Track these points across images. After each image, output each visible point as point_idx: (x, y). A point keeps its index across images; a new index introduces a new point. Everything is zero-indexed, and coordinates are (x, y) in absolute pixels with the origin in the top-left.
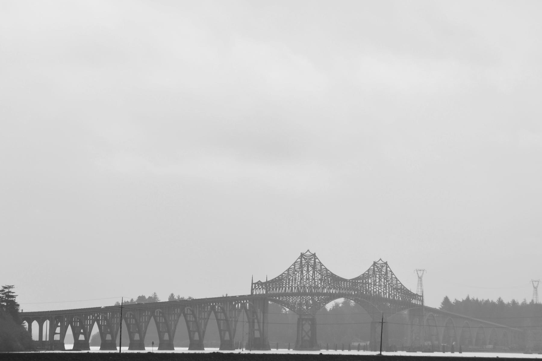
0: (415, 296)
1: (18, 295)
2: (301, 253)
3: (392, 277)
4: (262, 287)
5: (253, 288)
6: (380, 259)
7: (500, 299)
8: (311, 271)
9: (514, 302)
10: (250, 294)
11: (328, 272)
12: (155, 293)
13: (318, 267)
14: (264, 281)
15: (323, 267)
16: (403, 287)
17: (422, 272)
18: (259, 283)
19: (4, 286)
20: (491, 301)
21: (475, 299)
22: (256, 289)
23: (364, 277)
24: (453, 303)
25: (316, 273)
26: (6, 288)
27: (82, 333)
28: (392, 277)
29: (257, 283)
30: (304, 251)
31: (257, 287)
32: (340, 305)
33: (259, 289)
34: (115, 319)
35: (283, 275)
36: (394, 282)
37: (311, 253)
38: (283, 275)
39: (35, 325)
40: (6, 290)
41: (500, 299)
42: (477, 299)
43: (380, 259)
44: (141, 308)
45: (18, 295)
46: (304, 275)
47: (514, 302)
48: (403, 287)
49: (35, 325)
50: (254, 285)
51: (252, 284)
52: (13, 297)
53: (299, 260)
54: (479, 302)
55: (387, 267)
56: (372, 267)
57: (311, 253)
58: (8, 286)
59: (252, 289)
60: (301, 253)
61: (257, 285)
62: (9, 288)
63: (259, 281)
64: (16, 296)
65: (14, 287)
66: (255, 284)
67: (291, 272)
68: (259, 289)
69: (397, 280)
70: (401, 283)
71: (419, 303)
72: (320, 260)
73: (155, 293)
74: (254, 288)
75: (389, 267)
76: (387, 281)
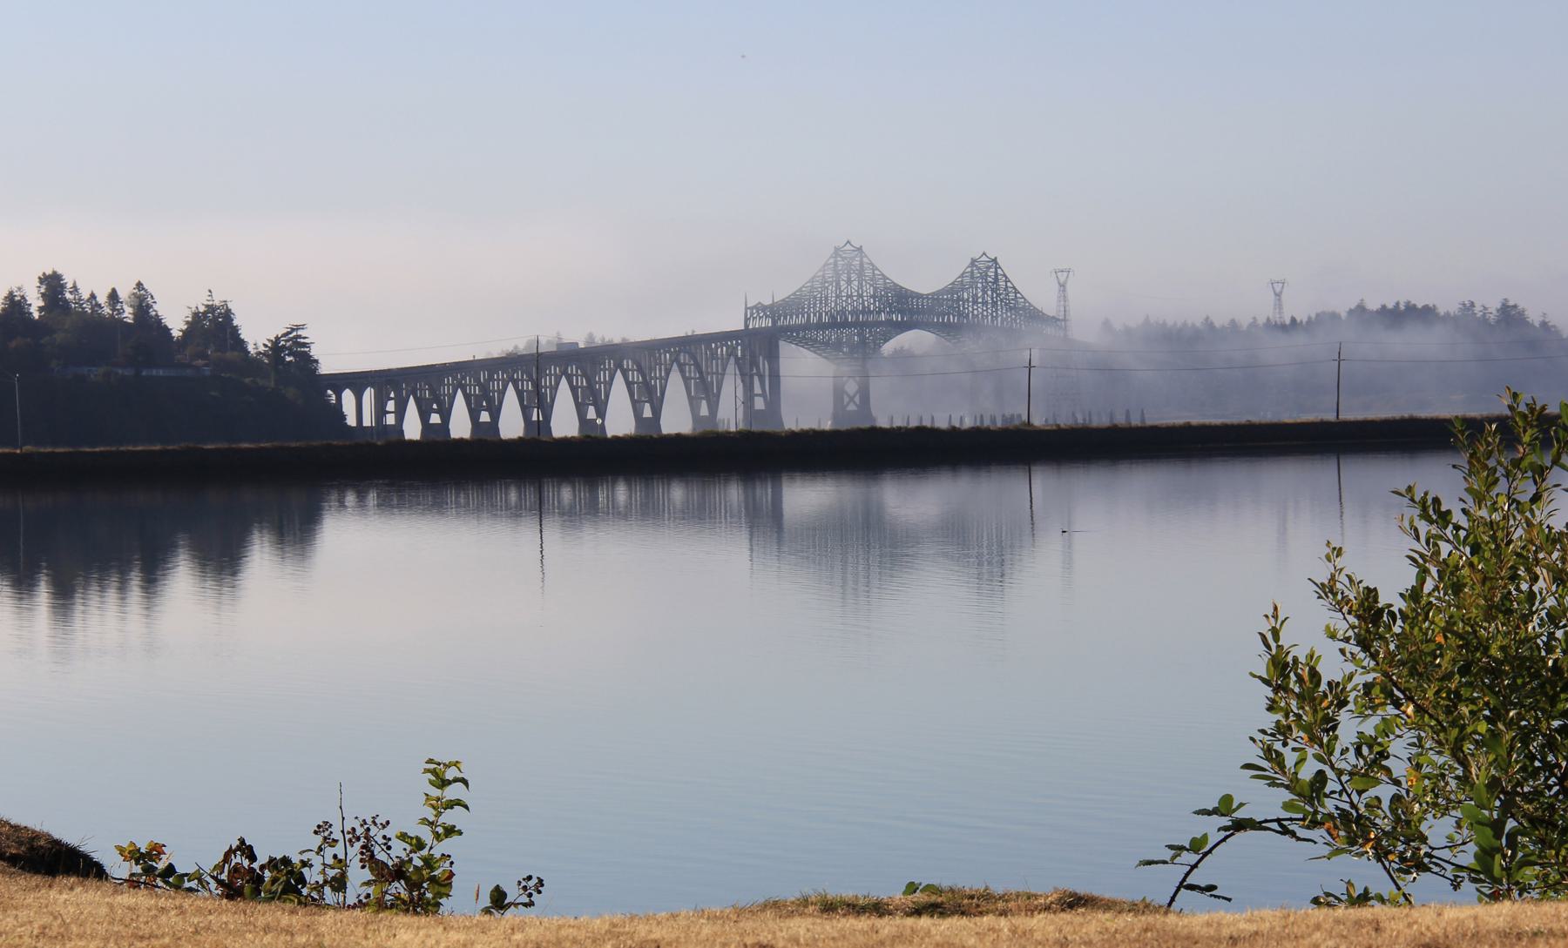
3: (1006, 285)
5: (749, 316)
6: (984, 254)
7: (1207, 318)
13: (868, 272)
14: (768, 302)
17: (1280, 285)
18: (760, 308)
22: (754, 318)
29: (755, 307)
31: (755, 316)
33: (760, 318)
43: (984, 254)
51: (746, 308)
52: (304, 345)
56: (832, 261)
59: (746, 319)
63: (760, 303)
66: (752, 308)
68: (760, 318)
70: (1023, 298)
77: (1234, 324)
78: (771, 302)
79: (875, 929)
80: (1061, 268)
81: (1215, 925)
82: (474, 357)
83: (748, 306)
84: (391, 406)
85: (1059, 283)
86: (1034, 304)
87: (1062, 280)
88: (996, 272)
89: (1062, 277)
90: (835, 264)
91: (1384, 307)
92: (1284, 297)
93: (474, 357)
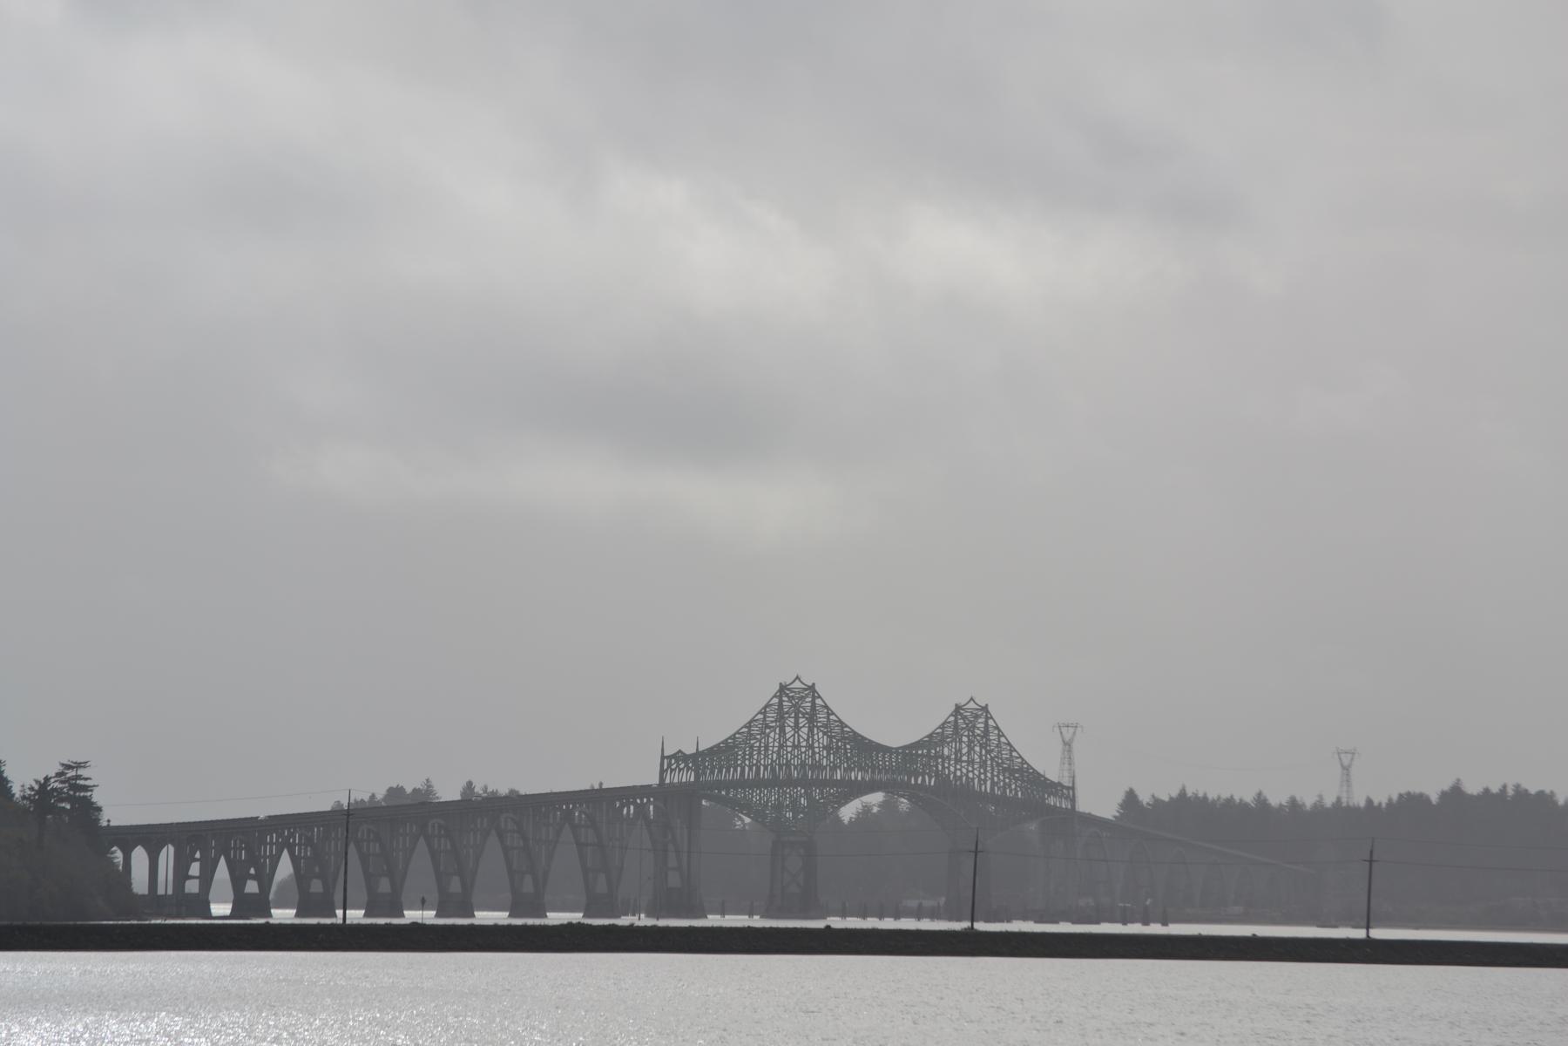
0: (1054, 788)
1: (97, 786)
2: (781, 684)
4: (687, 765)
5: (665, 767)
6: (797, 678)
7: (1260, 794)
8: (804, 726)
9: (1293, 802)
11: (845, 729)
12: (427, 780)
13: (822, 717)
15: (832, 717)
16: (1025, 766)
17: (1071, 730)
18: (679, 757)
19: (66, 762)
20: (1238, 801)
23: (933, 741)
24: (1148, 804)
25: (816, 732)
26: (68, 767)
27: (253, 877)
28: (999, 741)
31: (673, 767)
32: (875, 810)
35: (737, 736)
36: (1005, 754)
37: (804, 684)
38: (737, 736)
39: (140, 856)
40: (71, 773)
41: (1260, 794)
45: (97, 786)
46: (788, 736)
47: (1293, 802)
50: (666, 761)
51: (663, 757)
52: (86, 788)
53: (776, 700)
55: (988, 717)
56: (952, 719)
57: (804, 684)
58: (76, 763)
59: (662, 772)
60: (781, 684)
61: (673, 761)
62: (77, 767)
63: (680, 751)
64: (94, 786)
65: (88, 764)
66: (670, 757)
67: (755, 730)
69: (1012, 749)
70: (1021, 757)
71: (1065, 804)
73: (427, 780)
75: (992, 718)
76: (989, 752)
78: (695, 751)
83: (666, 754)
84: (195, 869)
85: (1064, 741)
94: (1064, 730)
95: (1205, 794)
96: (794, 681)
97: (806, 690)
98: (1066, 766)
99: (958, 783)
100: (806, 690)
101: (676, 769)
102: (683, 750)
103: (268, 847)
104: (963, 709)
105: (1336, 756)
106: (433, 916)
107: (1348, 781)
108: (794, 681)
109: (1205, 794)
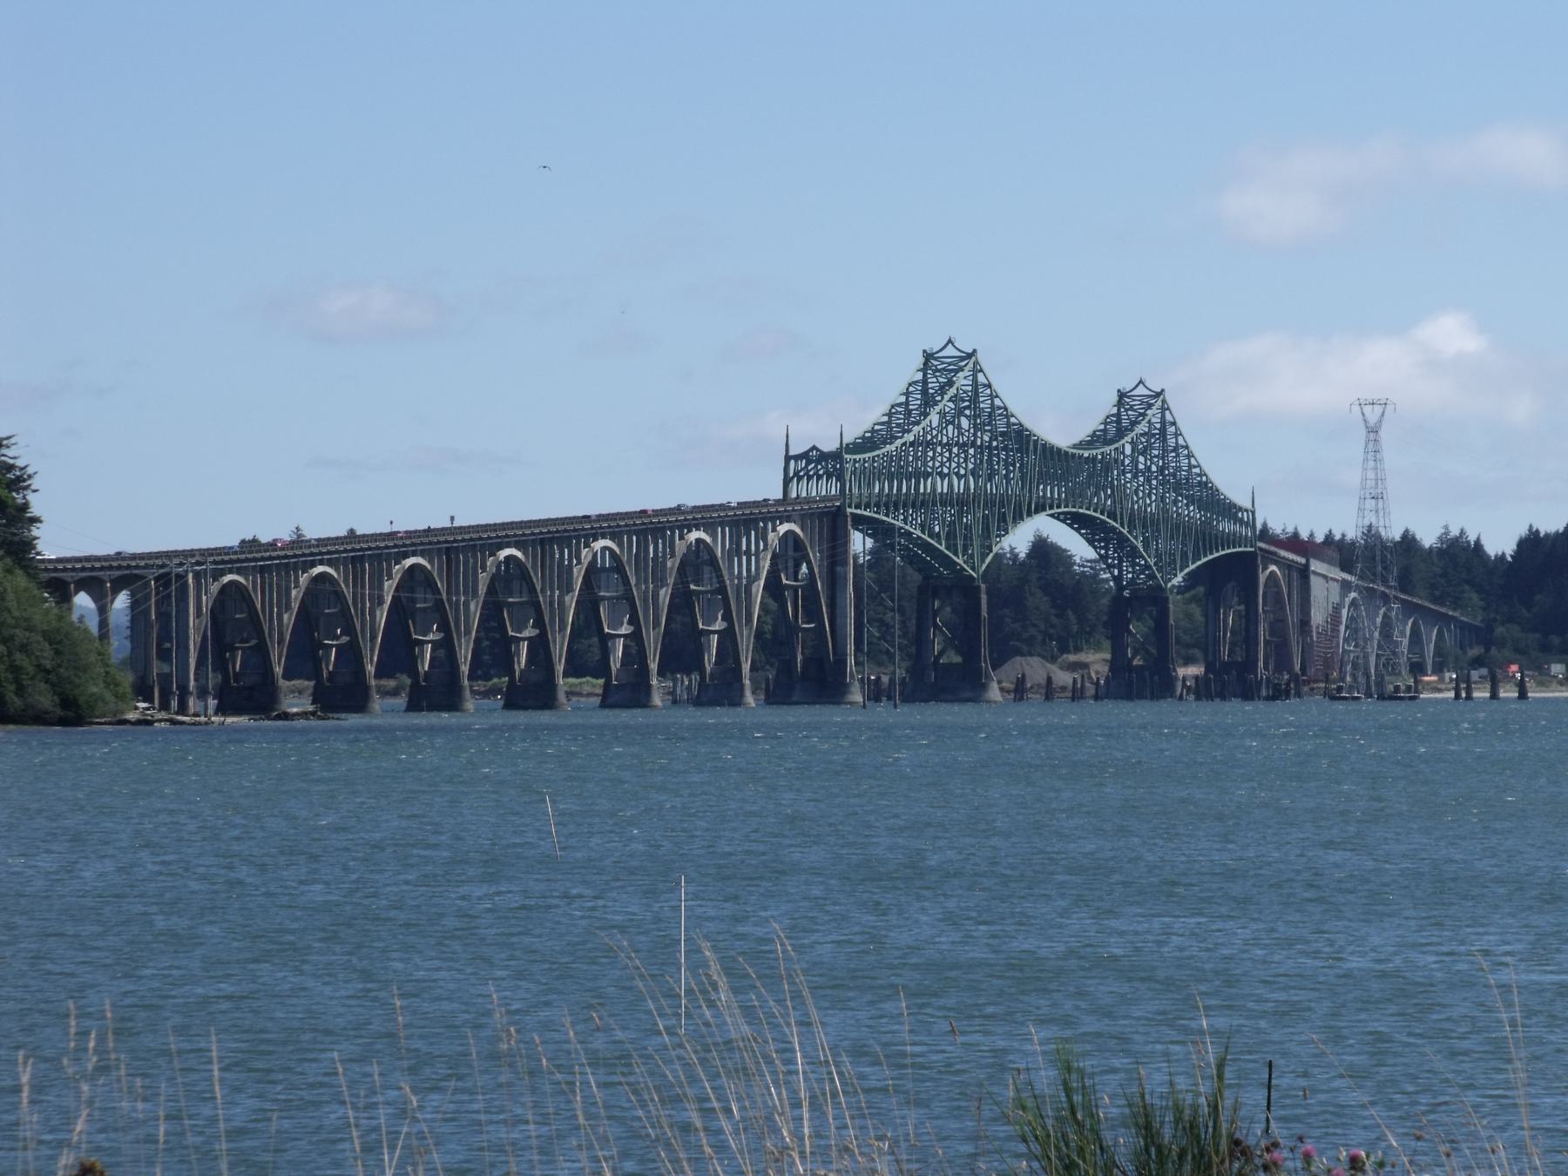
6: (950, 341)
10: (780, 496)
14: (829, 446)
18: (816, 457)
21: (1472, 538)
23: (902, 416)
30: (1127, 386)
31: (821, 472)
34: (744, 558)
35: (877, 427)
37: (960, 351)
42: (1296, 529)
44: (456, 545)
48: (1204, 479)
49: (83, 600)
50: (792, 462)
51: (788, 458)
53: (920, 376)
54: (1542, 535)
57: (960, 351)
59: (787, 482)
65: (13, 441)
66: (797, 458)
70: (1199, 466)
72: (1175, 415)
74: (793, 477)
75: (981, 371)
77: (1557, 532)
79: (1272, 1149)
80: (1370, 397)
81: (1534, 1133)
82: (452, 519)
83: (792, 452)
85: (1367, 427)
86: (1213, 480)
87: (1373, 419)
88: (1163, 417)
89: (1373, 414)
90: (925, 381)
91: (1296, 535)
92: (1384, 434)
93: (452, 519)
94: (1367, 409)
95: (1462, 532)
96: (1137, 386)
97: (962, 359)
98: (1372, 463)
99: (1136, 507)
100: (962, 359)
101: (803, 476)
102: (818, 446)
103: (744, 558)
104: (1129, 397)
105: (1356, 409)
106: (404, 708)
107: (393, 711)
108: (1137, 386)
109: (1462, 532)
